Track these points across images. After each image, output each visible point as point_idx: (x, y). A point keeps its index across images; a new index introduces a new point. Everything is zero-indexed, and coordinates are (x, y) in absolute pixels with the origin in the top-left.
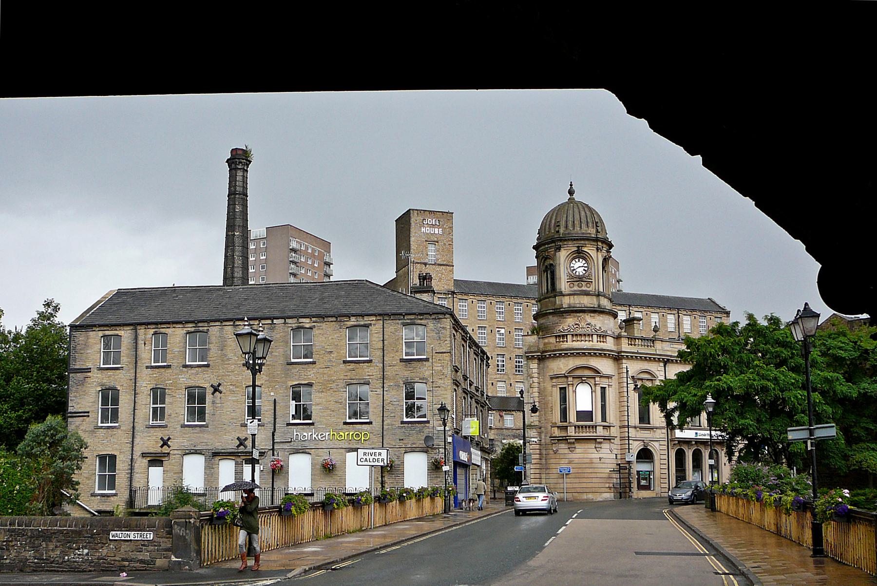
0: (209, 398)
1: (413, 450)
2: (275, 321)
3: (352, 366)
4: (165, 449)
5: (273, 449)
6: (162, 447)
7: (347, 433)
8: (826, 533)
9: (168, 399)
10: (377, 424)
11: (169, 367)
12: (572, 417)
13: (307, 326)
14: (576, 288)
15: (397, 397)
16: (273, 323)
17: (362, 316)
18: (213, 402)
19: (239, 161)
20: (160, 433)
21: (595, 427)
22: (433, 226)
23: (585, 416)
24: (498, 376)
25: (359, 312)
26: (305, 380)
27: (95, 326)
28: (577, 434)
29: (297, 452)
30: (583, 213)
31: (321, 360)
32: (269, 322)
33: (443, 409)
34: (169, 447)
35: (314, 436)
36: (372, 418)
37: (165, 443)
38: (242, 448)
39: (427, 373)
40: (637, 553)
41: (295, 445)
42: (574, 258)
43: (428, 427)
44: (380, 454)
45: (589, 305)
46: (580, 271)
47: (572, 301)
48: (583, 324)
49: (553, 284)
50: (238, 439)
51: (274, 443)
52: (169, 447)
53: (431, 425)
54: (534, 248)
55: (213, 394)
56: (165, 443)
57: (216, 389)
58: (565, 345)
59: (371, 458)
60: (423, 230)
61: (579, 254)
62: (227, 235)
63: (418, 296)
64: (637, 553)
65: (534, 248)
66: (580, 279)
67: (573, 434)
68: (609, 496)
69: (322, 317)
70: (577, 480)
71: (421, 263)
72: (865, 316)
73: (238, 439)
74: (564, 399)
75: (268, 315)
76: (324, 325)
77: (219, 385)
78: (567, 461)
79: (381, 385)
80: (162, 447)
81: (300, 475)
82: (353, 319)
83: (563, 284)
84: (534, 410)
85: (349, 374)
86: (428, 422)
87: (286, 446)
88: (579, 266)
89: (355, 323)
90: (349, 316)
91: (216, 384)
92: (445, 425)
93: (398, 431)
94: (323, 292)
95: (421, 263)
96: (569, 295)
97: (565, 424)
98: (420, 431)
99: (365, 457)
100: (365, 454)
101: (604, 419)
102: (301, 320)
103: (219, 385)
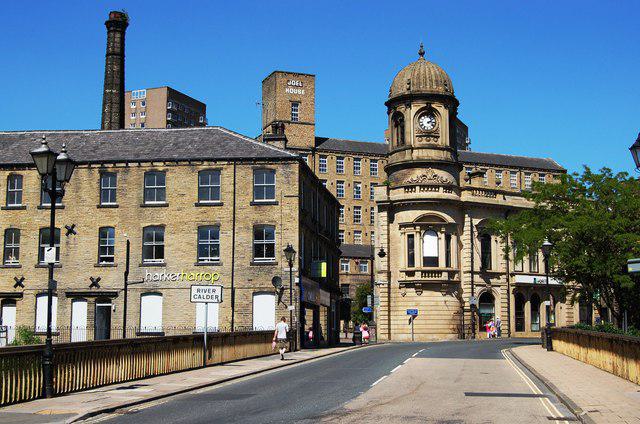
0: (63, 238)
2: (130, 164)
3: (204, 208)
4: (19, 290)
5: (125, 290)
6: (15, 286)
9: (22, 240)
10: (227, 265)
11: (24, 208)
12: (418, 263)
13: (161, 169)
14: (424, 142)
15: (246, 239)
16: (127, 166)
17: (215, 160)
18: (67, 243)
19: (118, 24)
20: (13, 273)
21: (440, 272)
23: (431, 261)
25: (211, 156)
27: (546, 385)
28: (423, 279)
32: (124, 165)
33: (289, 250)
34: (23, 287)
35: (165, 276)
36: (222, 257)
37: (19, 283)
40: (467, 394)
41: (148, 285)
42: (420, 117)
44: (214, 291)
46: (429, 127)
47: (420, 154)
48: (429, 176)
49: (403, 139)
50: (92, 279)
51: (126, 284)
52: (23, 287)
53: (279, 267)
54: (386, 104)
55: (67, 235)
56: (19, 283)
57: (71, 231)
60: (287, 90)
61: (429, 112)
62: (105, 93)
64: (467, 394)
65: (386, 104)
67: (420, 278)
68: (451, 337)
69: (176, 161)
70: (423, 322)
72: (342, 322)
73: (92, 279)
74: (411, 246)
75: (121, 157)
76: (177, 169)
77: (73, 226)
78: (414, 304)
80: (15, 286)
82: (205, 163)
83: (411, 138)
84: (382, 254)
87: (139, 286)
90: (203, 160)
91: (70, 225)
92: (291, 266)
93: (247, 272)
96: (418, 148)
98: (270, 272)
100: (198, 291)
101: (448, 264)
102: (155, 164)
103: (73, 226)
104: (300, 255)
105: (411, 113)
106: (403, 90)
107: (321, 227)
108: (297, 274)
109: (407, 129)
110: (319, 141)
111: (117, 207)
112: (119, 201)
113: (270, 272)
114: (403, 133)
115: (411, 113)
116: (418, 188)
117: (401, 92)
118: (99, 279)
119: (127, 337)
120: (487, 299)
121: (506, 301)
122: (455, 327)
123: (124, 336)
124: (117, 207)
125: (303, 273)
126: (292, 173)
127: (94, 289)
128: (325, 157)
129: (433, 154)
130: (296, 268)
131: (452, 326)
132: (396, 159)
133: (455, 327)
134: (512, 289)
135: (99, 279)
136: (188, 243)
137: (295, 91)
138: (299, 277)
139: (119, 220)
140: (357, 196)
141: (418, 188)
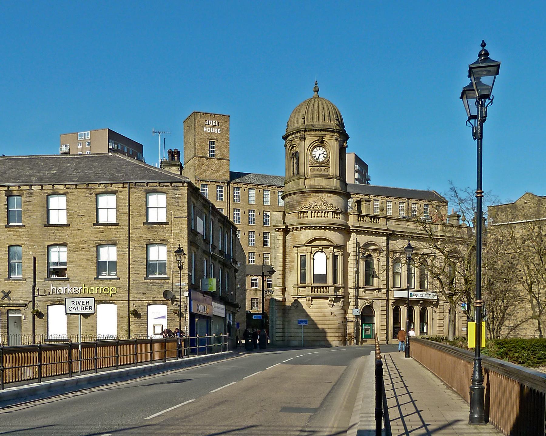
1: (155, 303)
7: (97, 288)
8: (238, 426)
10: (124, 281)
22: (213, 126)
23: (321, 278)
24: (264, 249)
26: (59, 240)
29: (54, 303)
30: (325, 107)
31: (74, 223)
35: (68, 290)
38: (6, 300)
39: (168, 235)
42: (315, 147)
43: (168, 284)
44: (87, 302)
45: (326, 187)
49: (297, 168)
50: (3, 292)
58: (305, 220)
59: (79, 307)
60: (205, 129)
63: (167, 169)
66: (320, 164)
71: (203, 157)
73: (3, 292)
74: (303, 265)
76: (76, 192)
79: (127, 245)
81: (58, 325)
83: (305, 168)
85: (98, 235)
86: (168, 278)
88: (319, 153)
89: (103, 190)
94: (79, 163)
95: (203, 157)
97: (304, 285)
99: (73, 306)
100: (73, 303)
101: (335, 281)
104: (190, 269)
105: (304, 146)
106: (298, 124)
107: (214, 247)
108: (187, 288)
109: (301, 161)
110: (234, 176)
111: (23, 226)
112: (25, 221)
113: (161, 286)
114: (297, 164)
115: (304, 146)
116: (309, 213)
117: (296, 126)
118: (10, 292)
119: (37, 341)
120: (367, 315)
121: (385, 313)
122: (340, 335)
123: (34, 342)
124: (23, 226)
125: (192, 287)
126: (182, 195)
127: (6, 300)
128: (238, 188)
129: (324, 183)
130: (185, 283)
131: (337, 334)
132: (291, 187)
133: (340, 335)
134: (391, 301)
135: (10, 292)
136: (88, 260)
137: (212, 130)
138: (189, 291)
139: (25, 238)
140: (251, 221)
141: (309, 213)
